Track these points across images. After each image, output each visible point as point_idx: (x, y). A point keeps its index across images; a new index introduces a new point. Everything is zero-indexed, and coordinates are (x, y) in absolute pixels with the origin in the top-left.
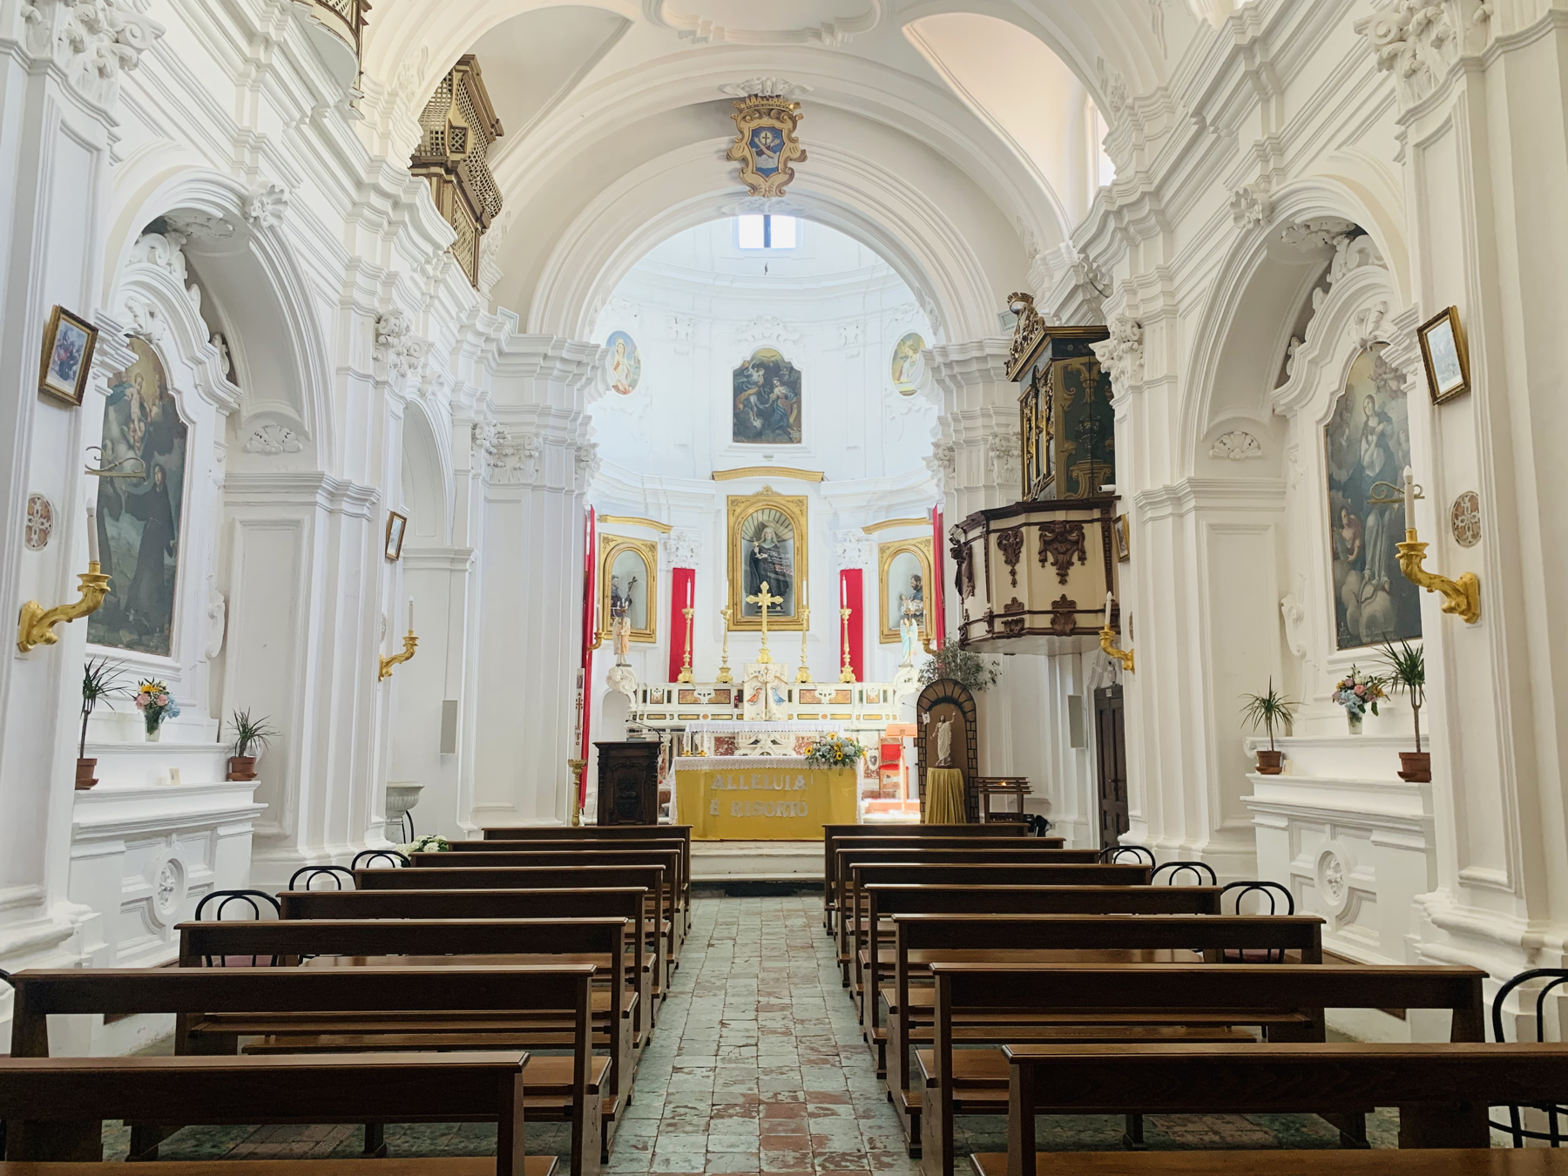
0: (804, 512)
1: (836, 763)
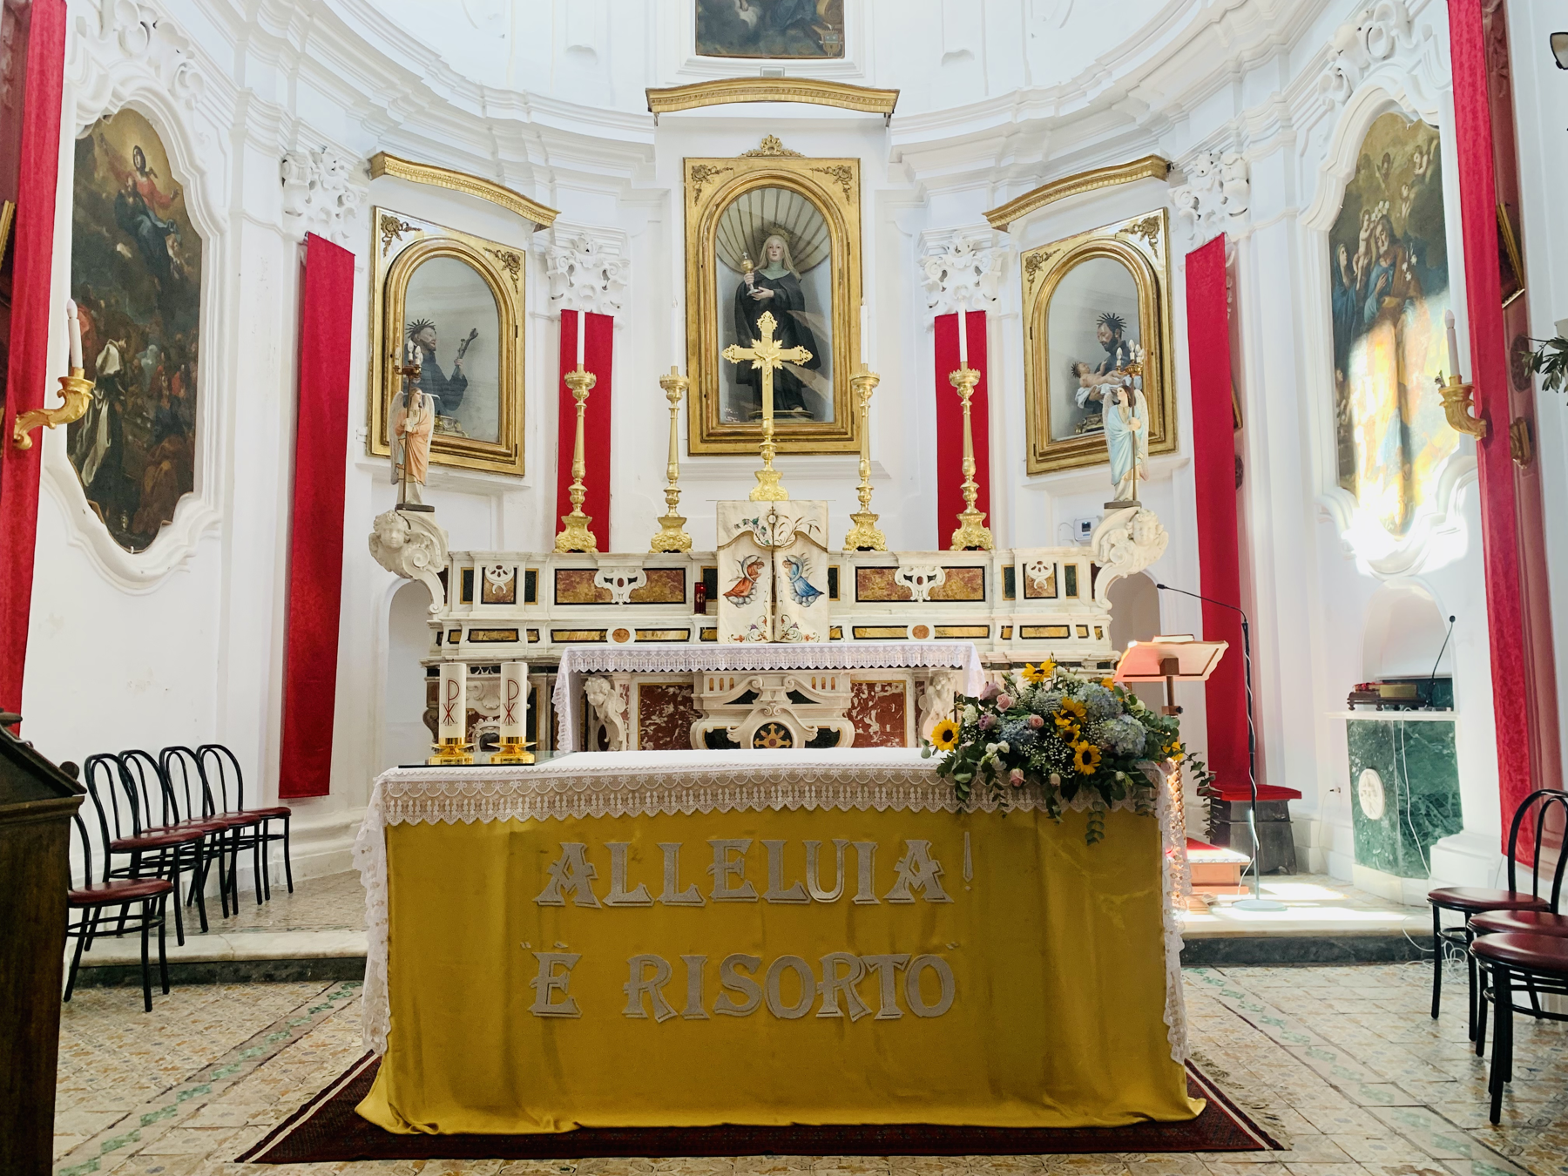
1: (1069, 789)
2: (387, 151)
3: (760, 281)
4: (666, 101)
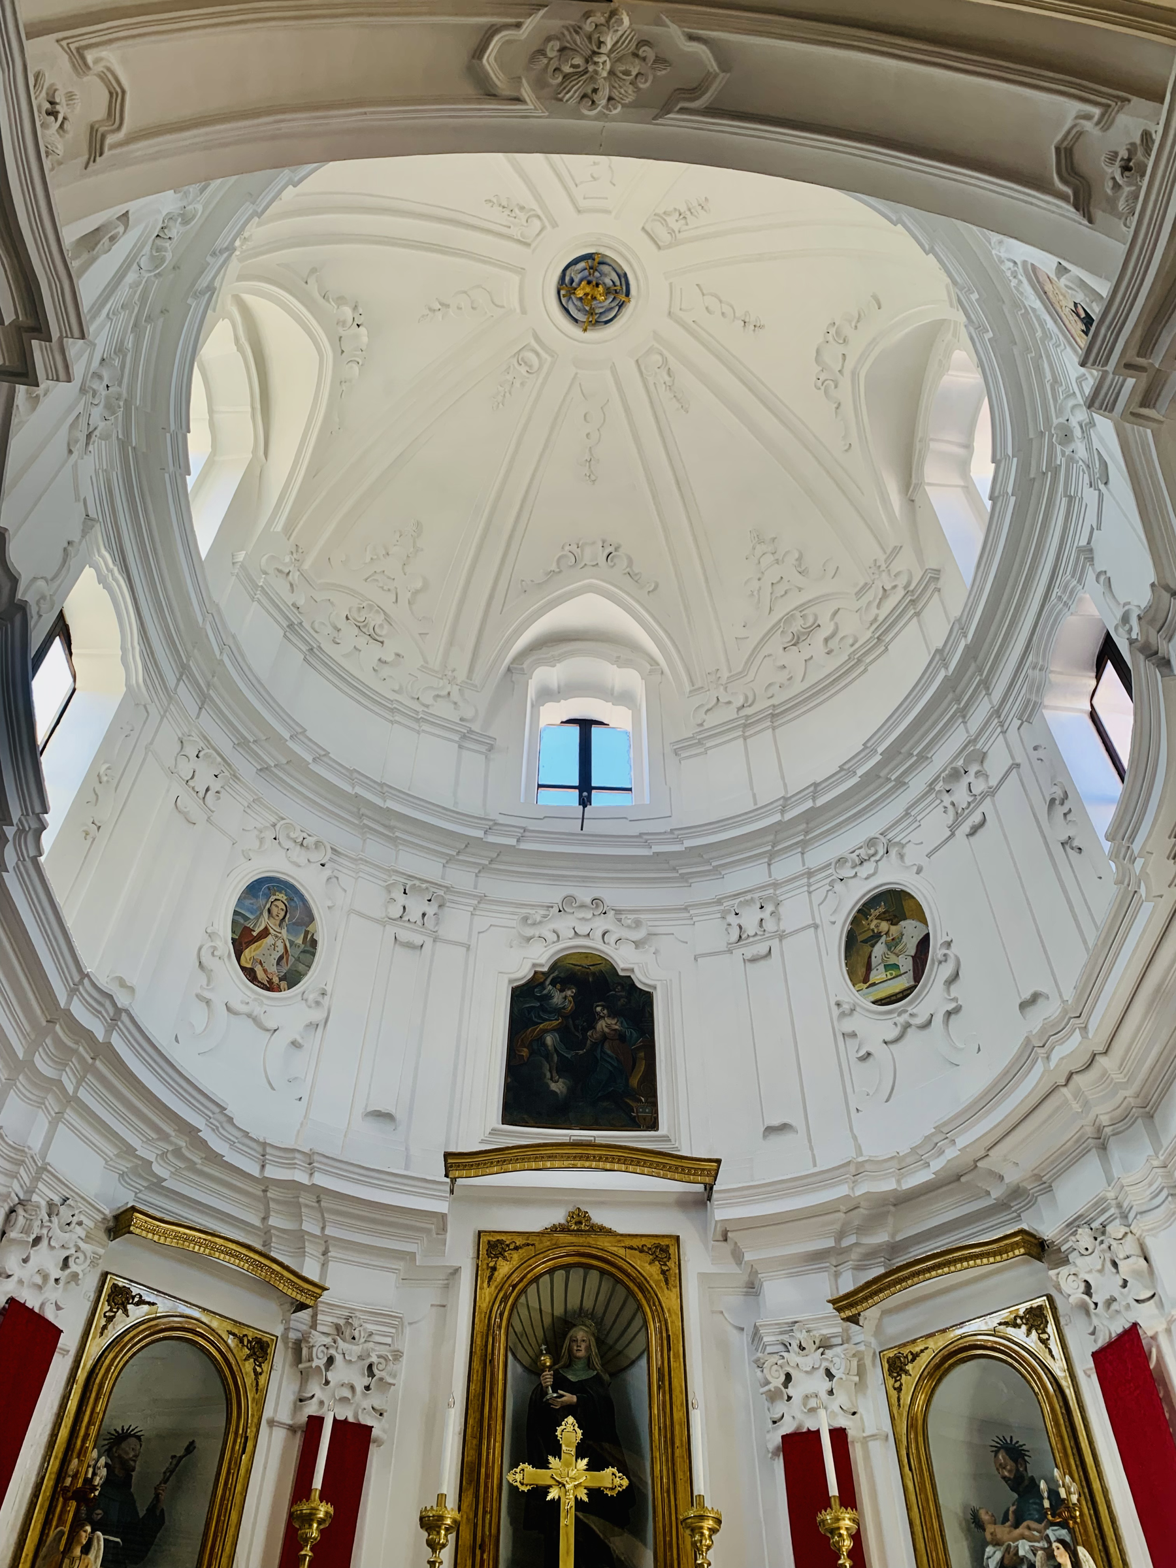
0: (672, 1277)
2: (138, 1206)
3: (560, 1383)
4: (465, 1166)
